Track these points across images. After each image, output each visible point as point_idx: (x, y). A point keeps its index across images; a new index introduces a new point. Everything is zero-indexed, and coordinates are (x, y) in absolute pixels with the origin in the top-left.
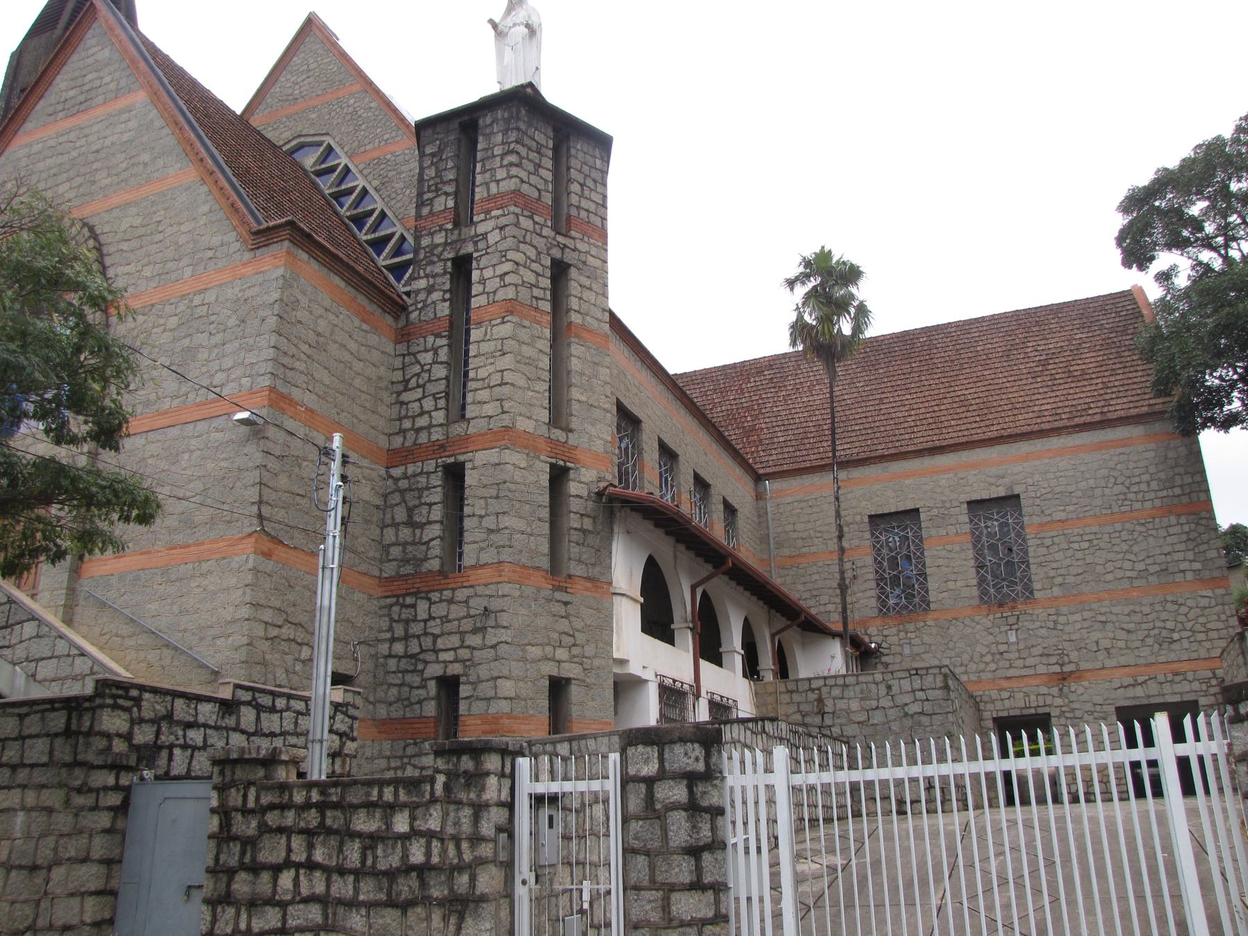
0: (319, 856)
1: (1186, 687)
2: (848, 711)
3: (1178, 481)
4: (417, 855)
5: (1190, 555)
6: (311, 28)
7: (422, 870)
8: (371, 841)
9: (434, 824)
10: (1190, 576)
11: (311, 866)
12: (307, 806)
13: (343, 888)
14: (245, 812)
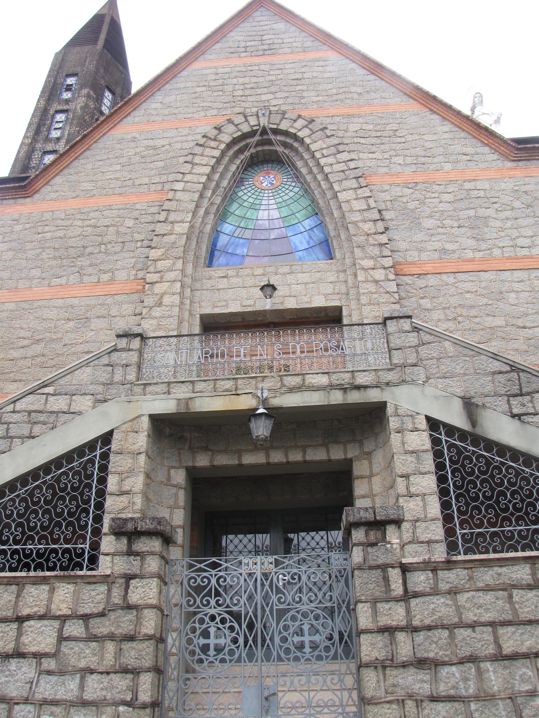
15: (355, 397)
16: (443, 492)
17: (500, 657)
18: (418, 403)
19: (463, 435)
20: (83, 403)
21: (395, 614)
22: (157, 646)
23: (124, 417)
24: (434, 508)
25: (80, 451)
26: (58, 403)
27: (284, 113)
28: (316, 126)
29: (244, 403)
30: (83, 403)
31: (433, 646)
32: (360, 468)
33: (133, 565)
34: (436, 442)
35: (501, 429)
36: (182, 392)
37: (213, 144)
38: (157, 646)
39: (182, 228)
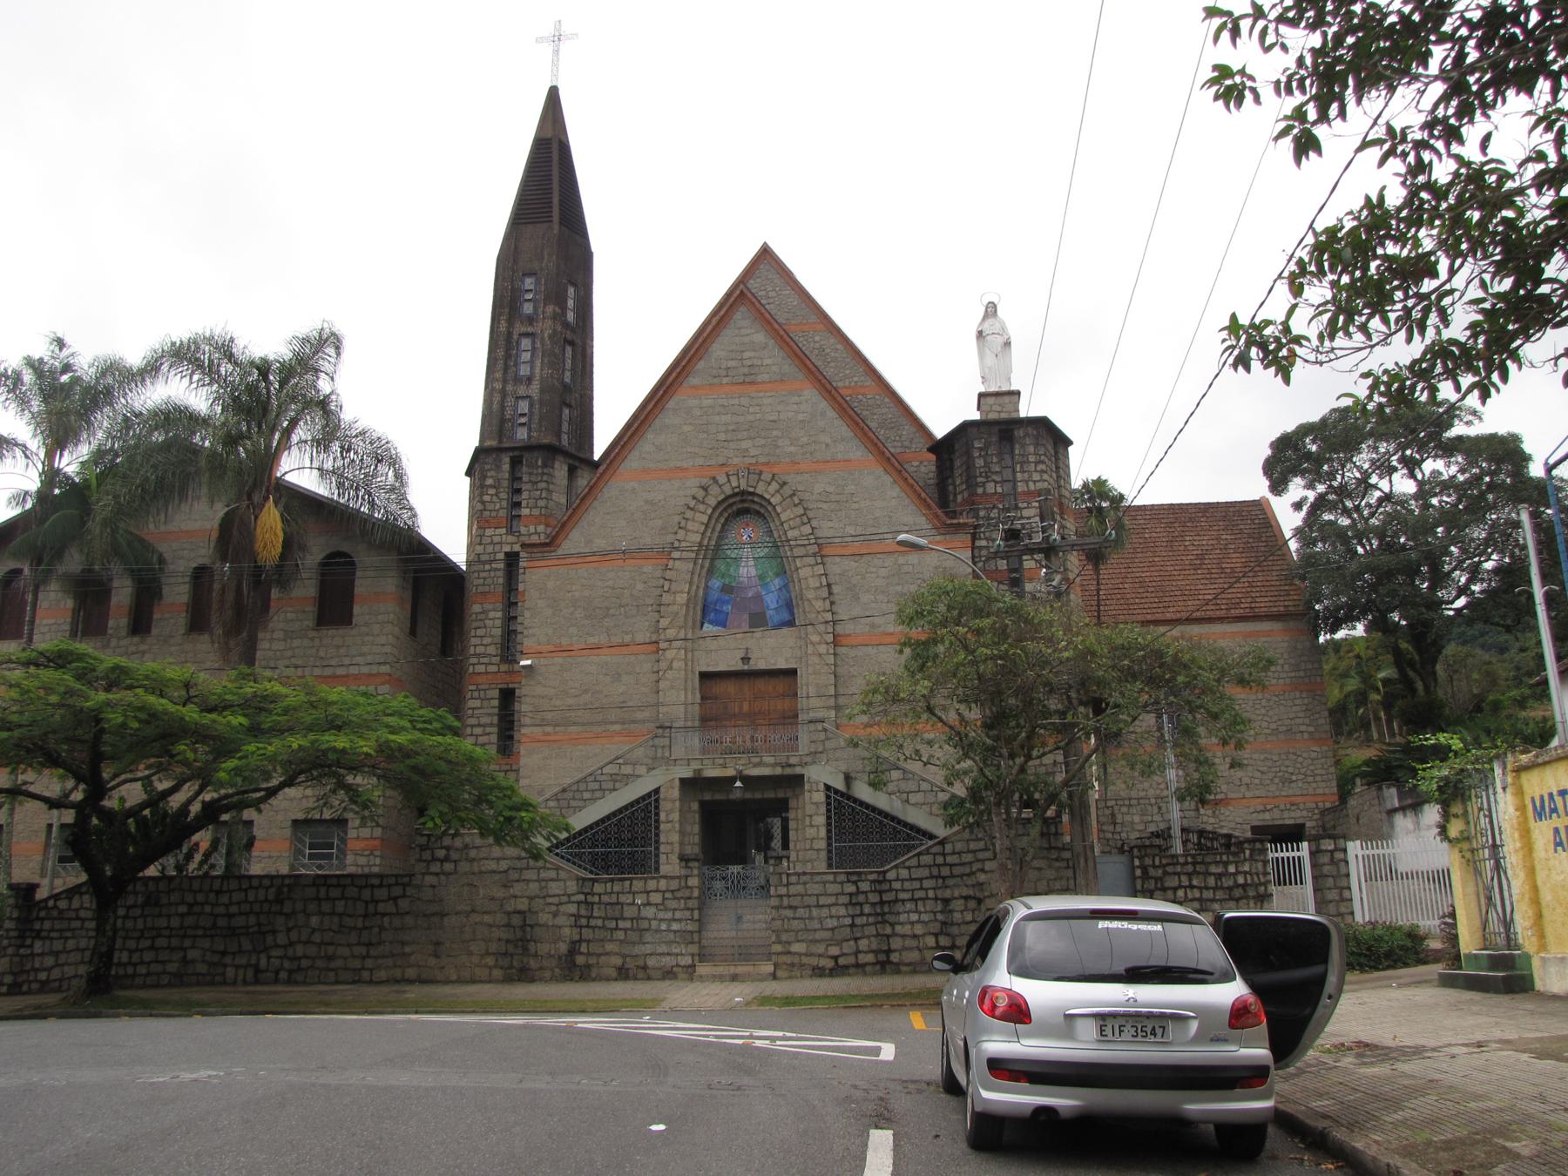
0: (1195, 882)
1: (1298, 813)
2: (1132, 823)
3: (1303, 666)
4: (1241, 880)
5: (1307, 721)
6: (765, 254)
7: (1244, 886)
8: (1219, 876)
9: (1246, 868)
10: (1306, 736)
11: (1192, 887)
12: (1187, 863)
13: (1208, 894)
14: (1154, 866)
15: (788, 771)
16: (829, 824)
17: (818, 906)
18: (822, 775)
19: (842, 794)
20: (642, 770)
21: (783, 891)
22: (227, 644)
23: (665, 779)
24: (823, 832)
25: (643, 798)
26: (627, 770)
27: (760, 473)
28: (787, 491)
29: (730, 772)
30: (642, 770)
31: (796, 901)
32: (792, 803)
33: (688, 872)
34: (828, 797)
35: (863, 792)
36: (696, 766)
37: (702, 507)
38: (227, 644)
39: (682, 598)
